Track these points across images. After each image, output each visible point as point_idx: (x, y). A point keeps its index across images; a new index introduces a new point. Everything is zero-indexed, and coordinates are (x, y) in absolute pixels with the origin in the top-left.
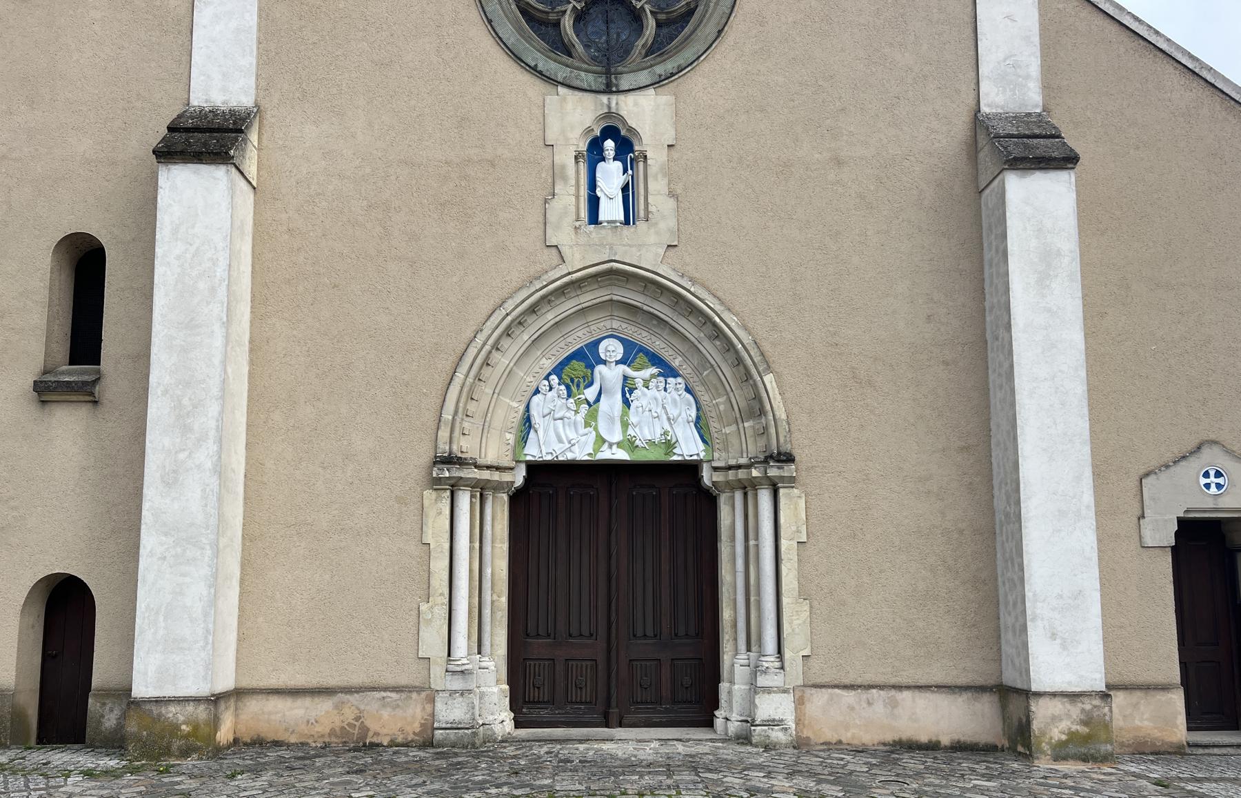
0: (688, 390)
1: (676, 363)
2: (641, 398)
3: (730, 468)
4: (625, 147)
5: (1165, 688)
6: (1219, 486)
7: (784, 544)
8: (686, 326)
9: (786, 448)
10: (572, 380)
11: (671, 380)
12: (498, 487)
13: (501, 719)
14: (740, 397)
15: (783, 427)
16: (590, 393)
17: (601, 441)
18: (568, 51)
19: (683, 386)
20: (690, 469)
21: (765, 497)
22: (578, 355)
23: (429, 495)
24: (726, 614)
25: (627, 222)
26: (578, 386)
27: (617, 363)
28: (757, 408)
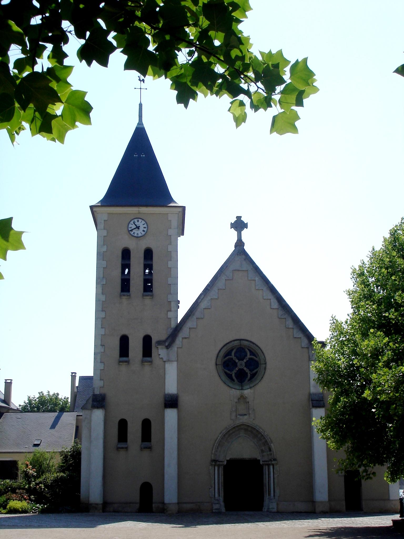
12: (221, 465)
15: (275, 454)
18: (233, 380)
21: (271, 467)
23: (211, 467)
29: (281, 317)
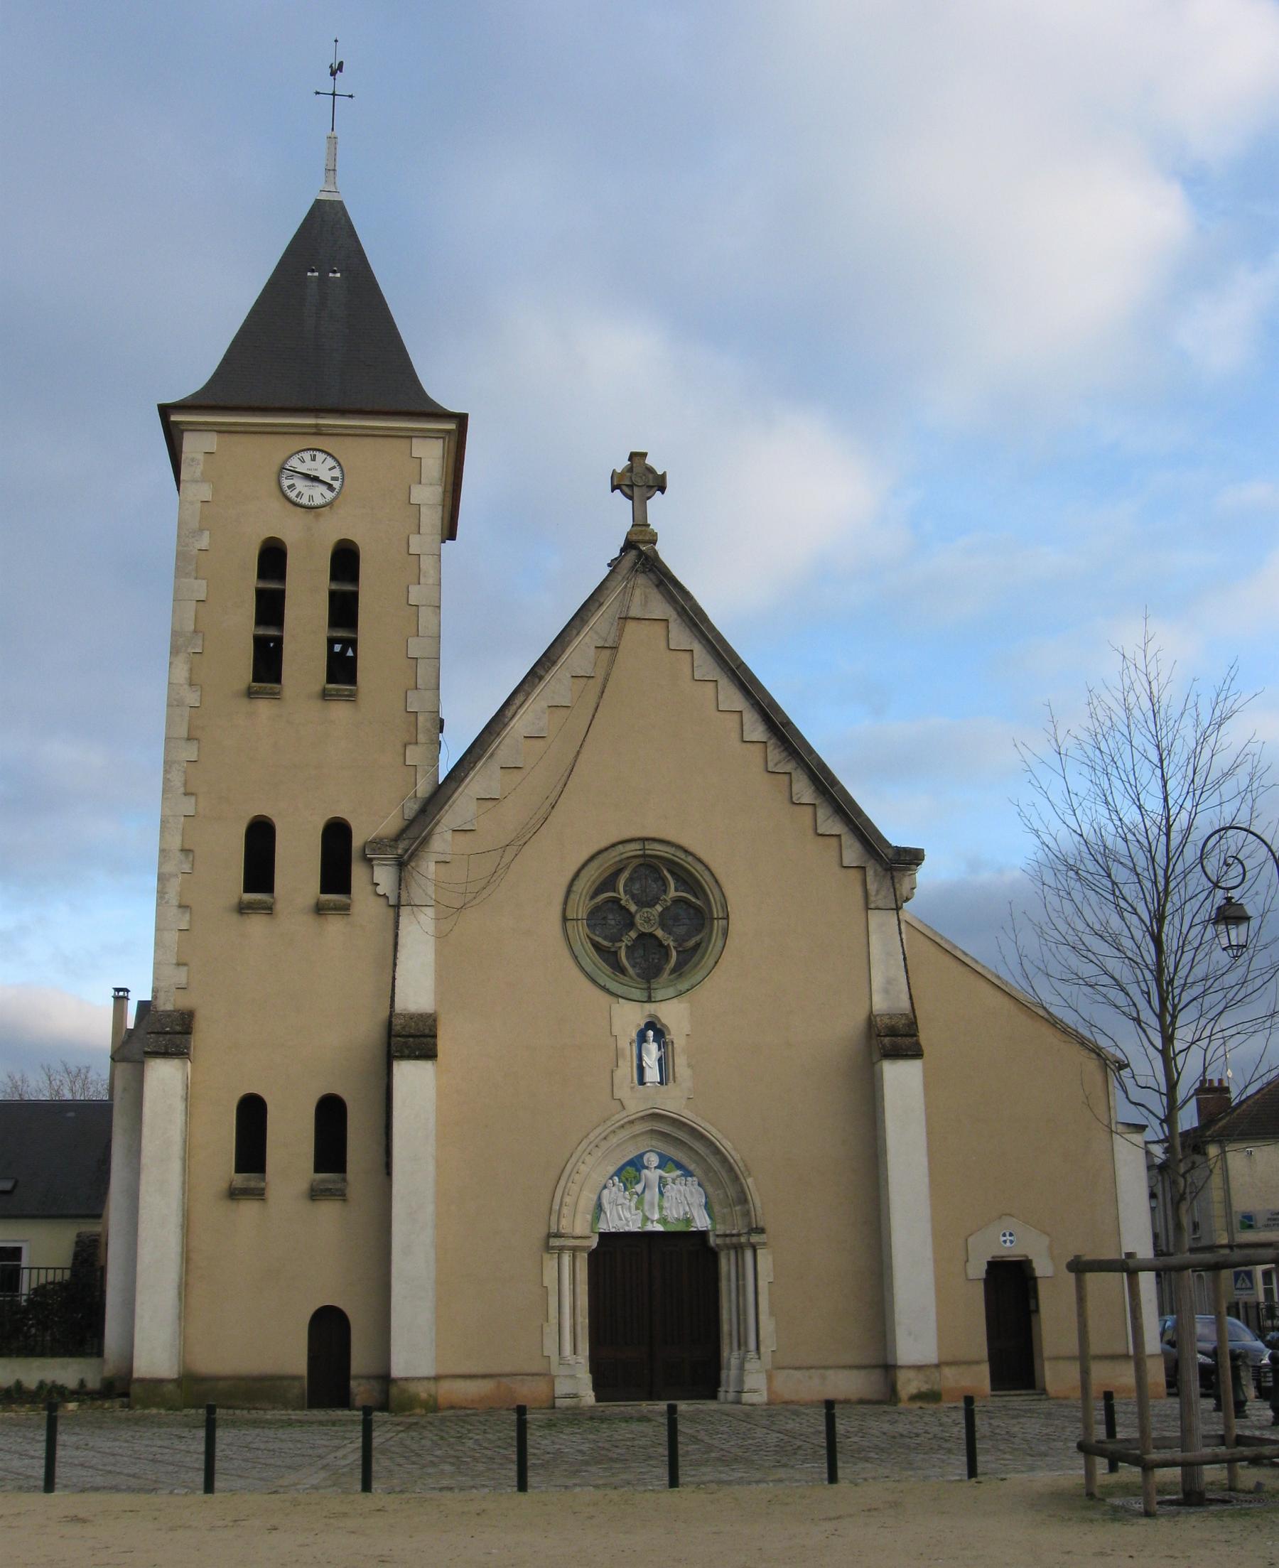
0: (699, 1185)
1: (692, 1167)
2: (672, 1191)
3: (726, 1236)
4: (660, 1034)
5: (978, 1363)
6: (1011, 1242)
7: (761, 1283)
8: (697, 1146)
9: (761, 1224)
10: (627, 1179)
11: (689, 1179)
13: (589, 1397)
14: (732, 1192)
16: (639, 1188)
17: (646, 1219)
19: (696, 1183)
20: (702, 1235)
22: (631, 1163)
24: (725, 1328)
25: (661, 1083)
26: (631, 1183)
27: (656, 1168)
28: (743, 1199)
29: (774, 770)
